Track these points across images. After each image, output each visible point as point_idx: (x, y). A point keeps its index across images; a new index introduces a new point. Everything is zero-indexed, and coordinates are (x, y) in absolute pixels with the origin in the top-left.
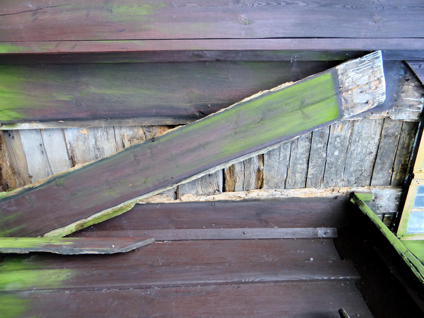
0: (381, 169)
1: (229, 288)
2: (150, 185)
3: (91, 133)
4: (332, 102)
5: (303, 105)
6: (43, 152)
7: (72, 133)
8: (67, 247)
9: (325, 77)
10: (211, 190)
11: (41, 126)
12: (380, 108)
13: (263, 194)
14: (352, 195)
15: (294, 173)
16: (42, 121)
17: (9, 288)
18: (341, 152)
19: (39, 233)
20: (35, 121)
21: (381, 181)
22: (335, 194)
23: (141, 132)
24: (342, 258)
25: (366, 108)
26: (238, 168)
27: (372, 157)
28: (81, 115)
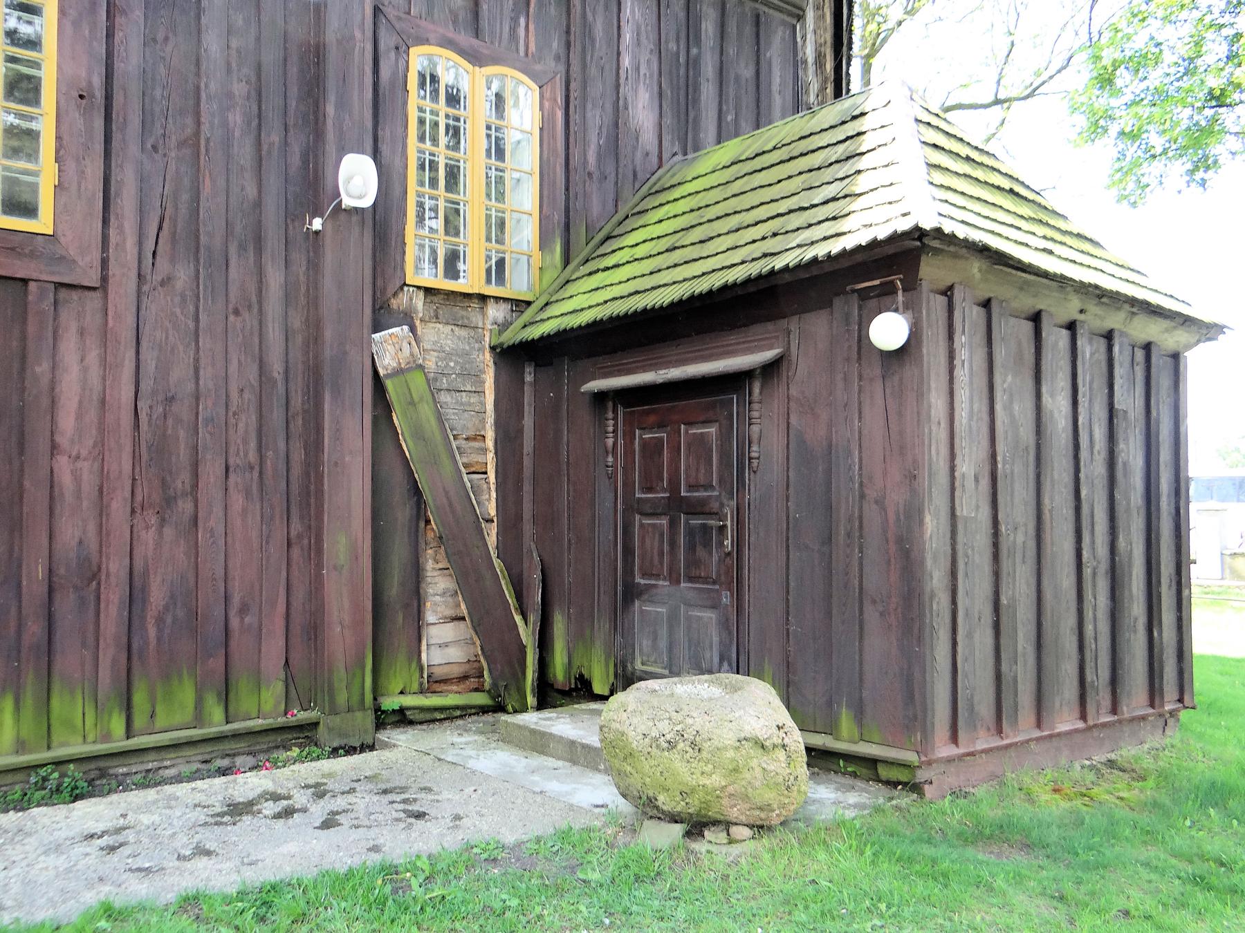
0: (468, 319)
1: (571, 472)
2: (480, 544)
3: (431, 598)
4: (409, 376)
5: (412, 403)
6: (446, 645)
7: (430, 617)
8: (534, 617)
9: (389, 384)
10: (485, 486)
11: (424, 643)
12: (413, 329)
13: (490, 435)
14: (493, 348)
15: (470, 404)
16: (420, 641)
17: (566, 660)
18: (451, 360)
19: (523, 649)
20: (419, 646)
21: (480, 317)
22: (491, 364)
23: (430, 551)
24: (551, 364)
25: (414, 343)
26: (465, 460)
27: (456, 329)
28: (416, 604)
